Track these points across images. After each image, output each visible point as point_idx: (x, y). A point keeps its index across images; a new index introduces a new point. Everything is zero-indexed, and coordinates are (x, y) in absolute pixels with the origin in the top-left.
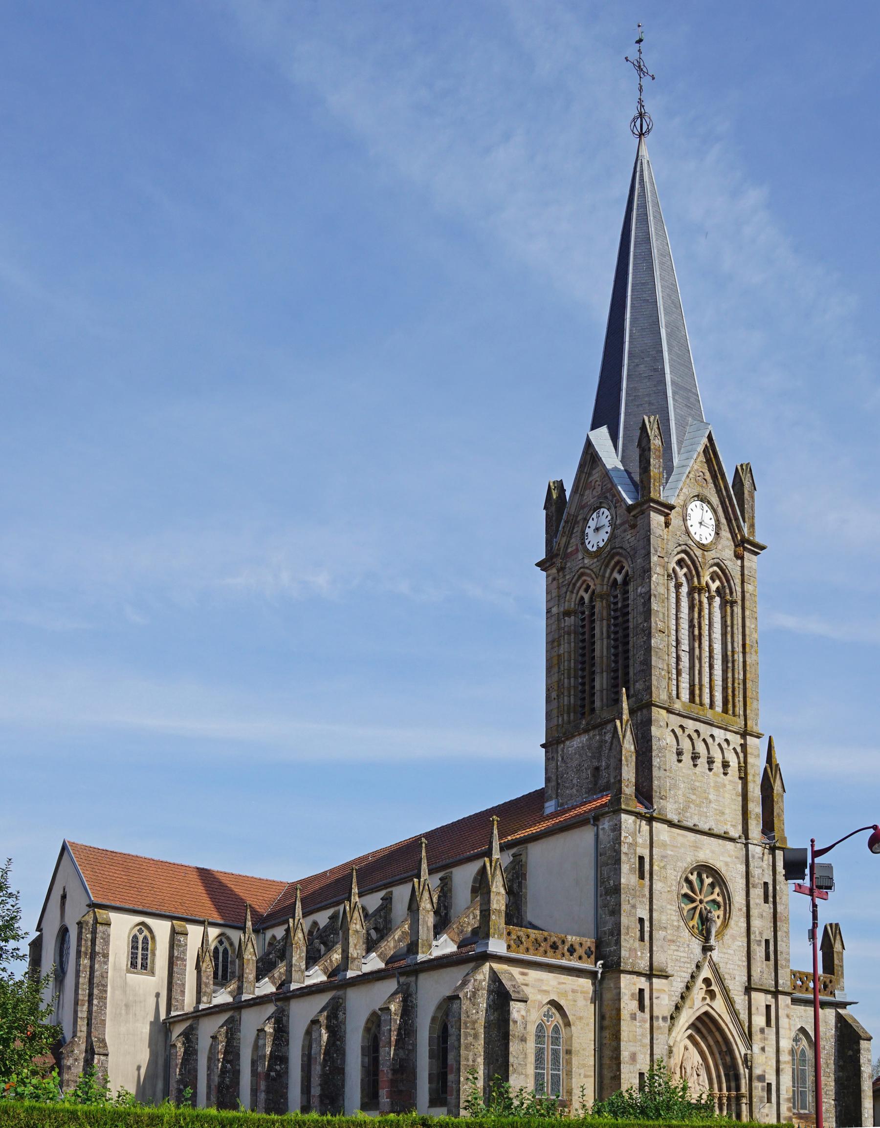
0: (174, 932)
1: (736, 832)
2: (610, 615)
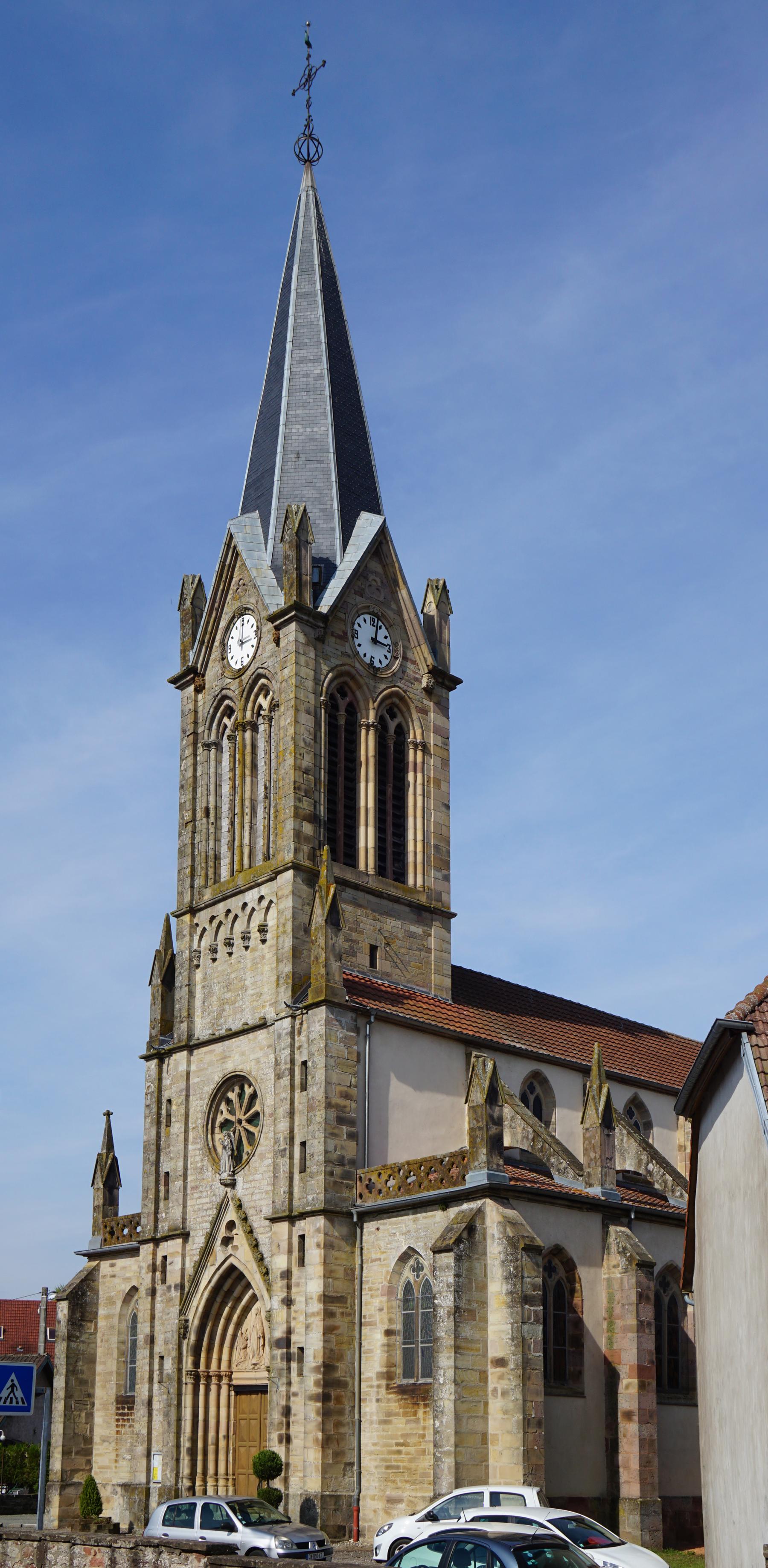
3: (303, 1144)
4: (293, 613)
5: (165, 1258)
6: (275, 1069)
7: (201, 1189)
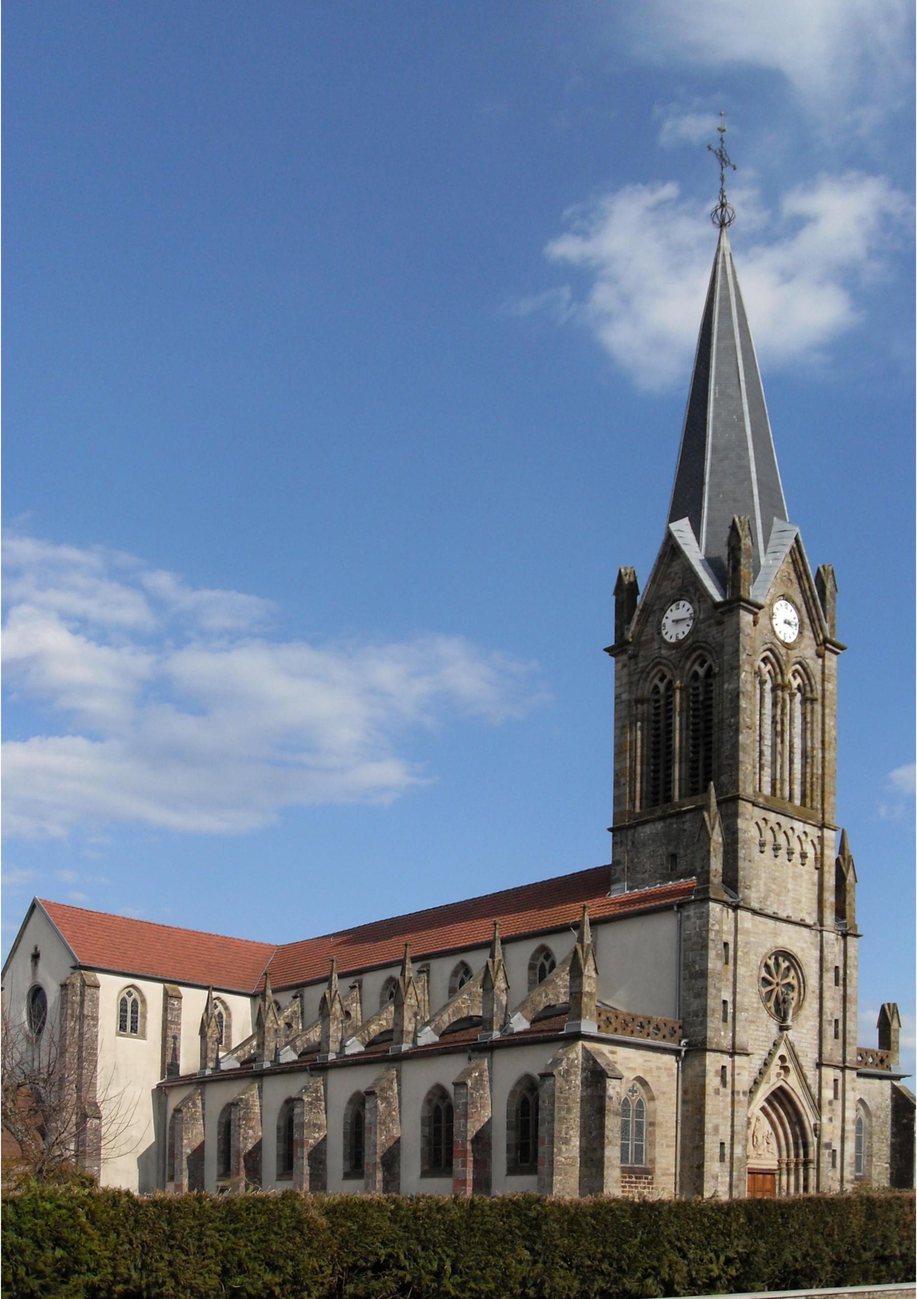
0: (167, 996)
1: (809, 921)
2: (689, 706)
7: (757, 1024)
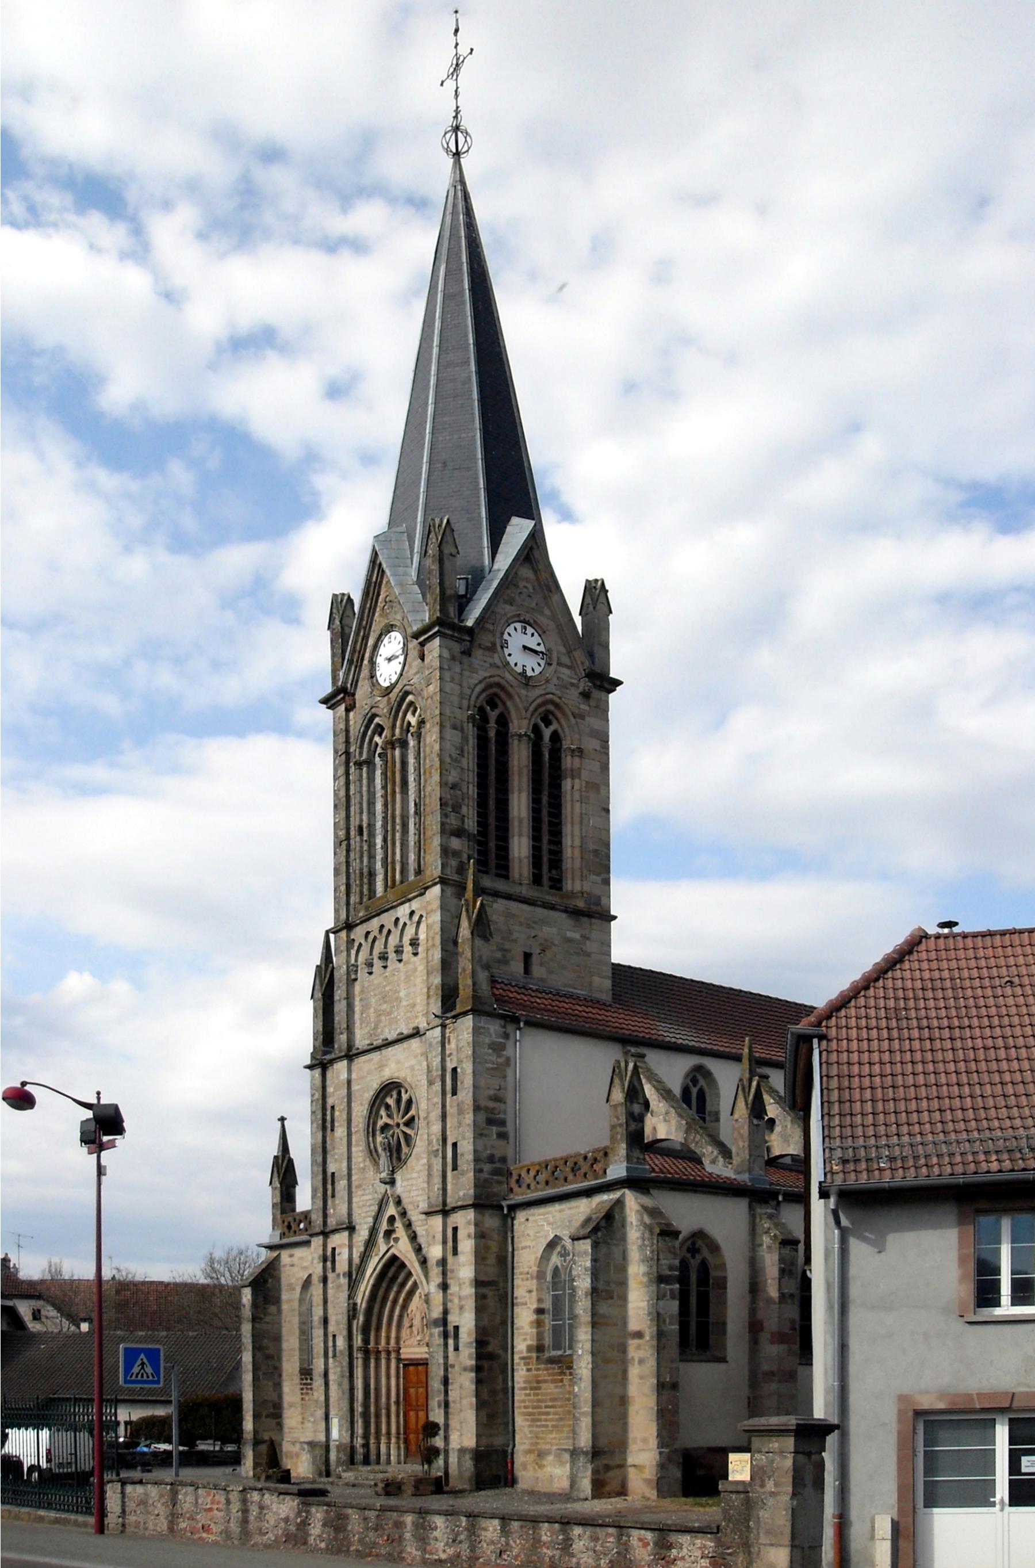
3: (455, 1145)
4: (436, 629)
5: (334, 1249)
6: (427, 1076)
